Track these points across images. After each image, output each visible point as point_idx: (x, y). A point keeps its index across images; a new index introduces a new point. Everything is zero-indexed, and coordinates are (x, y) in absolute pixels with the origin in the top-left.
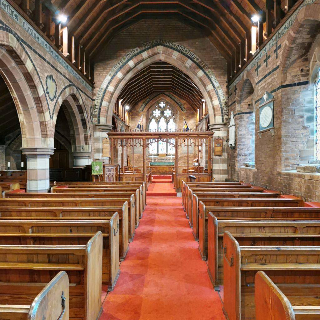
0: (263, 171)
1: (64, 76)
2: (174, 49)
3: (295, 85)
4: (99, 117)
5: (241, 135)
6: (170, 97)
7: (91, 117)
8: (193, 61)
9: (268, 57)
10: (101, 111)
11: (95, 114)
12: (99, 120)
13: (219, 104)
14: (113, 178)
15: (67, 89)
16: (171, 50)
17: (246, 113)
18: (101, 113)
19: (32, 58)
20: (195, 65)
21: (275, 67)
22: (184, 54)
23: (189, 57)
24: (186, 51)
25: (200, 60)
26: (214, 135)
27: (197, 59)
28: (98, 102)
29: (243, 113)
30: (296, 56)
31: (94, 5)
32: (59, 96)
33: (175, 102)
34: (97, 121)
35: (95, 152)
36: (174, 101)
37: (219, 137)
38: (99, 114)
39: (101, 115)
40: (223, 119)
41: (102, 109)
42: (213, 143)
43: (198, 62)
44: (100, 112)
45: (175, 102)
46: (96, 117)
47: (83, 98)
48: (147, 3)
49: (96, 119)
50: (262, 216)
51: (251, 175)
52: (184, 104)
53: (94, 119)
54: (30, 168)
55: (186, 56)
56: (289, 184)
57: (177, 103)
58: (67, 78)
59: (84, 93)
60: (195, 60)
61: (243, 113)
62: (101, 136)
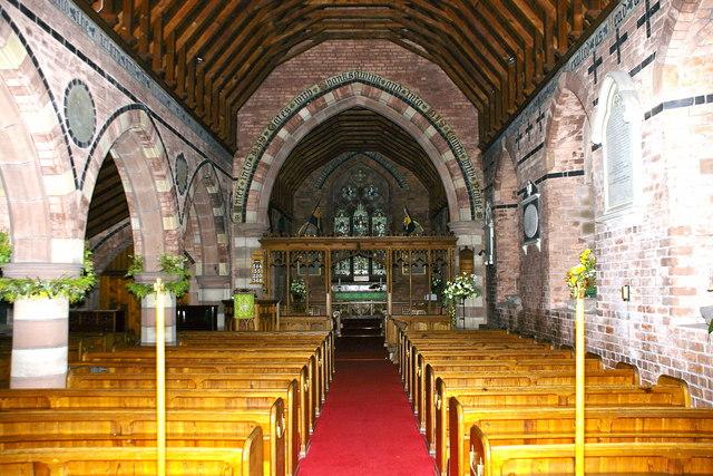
0: (529, 310)
1: (198, 151)
2: (382, 89)
3: (565, 174)
4: (245, 211)
5: (503, 244)
8: (417, 110)
9: (531, 127)
12: (244, 216)
15: (123, 116)
16: (376, 90)
17: (509, 206)
19: (23, 31)
20: (419, 116)
21: (539, 144)
22: (400, 97)
23: (409, 103)
24: (404, 92)
25: (428, 107)
27: (424, 107)
28: (242, 184)
29: (505, 207)
30: (566, 133)
31: (238, 10)
32: (101, 133)
38: (245, 205)
40: (473, 213)
42: (457, 258)
43: (425, 111)
44: (246, 201)
47: (221, 179)
49: (240, 214)
51: (515, 316)
54: (149, 306)
55: (405, 100)
56: (559, 328)
58: (200, 153)
59: (222, 171)
60: (421, 107)
61: (505, 207)
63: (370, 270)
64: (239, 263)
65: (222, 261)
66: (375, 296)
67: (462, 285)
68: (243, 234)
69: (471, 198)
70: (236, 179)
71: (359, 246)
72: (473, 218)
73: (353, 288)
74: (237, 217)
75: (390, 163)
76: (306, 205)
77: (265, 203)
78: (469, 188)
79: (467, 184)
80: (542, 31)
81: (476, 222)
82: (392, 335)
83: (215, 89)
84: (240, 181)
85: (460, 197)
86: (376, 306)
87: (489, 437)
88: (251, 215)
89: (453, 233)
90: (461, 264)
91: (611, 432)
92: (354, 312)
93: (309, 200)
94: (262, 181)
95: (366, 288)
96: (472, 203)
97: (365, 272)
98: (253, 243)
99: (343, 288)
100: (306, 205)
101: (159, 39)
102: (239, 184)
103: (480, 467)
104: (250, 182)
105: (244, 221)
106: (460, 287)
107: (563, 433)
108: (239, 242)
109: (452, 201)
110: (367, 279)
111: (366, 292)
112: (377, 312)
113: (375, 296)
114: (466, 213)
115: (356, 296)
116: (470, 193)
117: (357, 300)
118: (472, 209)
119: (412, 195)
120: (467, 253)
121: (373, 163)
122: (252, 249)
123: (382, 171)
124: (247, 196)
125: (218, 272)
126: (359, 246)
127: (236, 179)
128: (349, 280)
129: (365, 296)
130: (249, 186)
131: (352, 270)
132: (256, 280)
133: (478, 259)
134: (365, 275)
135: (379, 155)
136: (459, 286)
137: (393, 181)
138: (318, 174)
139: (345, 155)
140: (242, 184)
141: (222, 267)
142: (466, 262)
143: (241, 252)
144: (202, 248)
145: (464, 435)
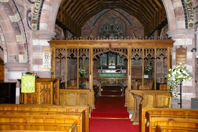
4: (39, 23)
6: (120, 13)
7: (29, 22)
10: (41, 16)
11: (35, 19)
12: (38, 26)
13: (182, 5)
14: (50, 96)
18: (41, 18)
26: (175, 44)
28: (37, 5)
33: (125, 17)
34: (36, 27)
35: (33, 63)
36: (123, 16)
37: (181, 46)
38: (39, 19)
39: (40, 21)
40: (186, 24)
41: (42, 13)
44: (39, 16)
45: (125, 17)
46: (35, 23)
48: (106, 118)
49: (36, 25)
50: (147, 106)
52: (133, 19)
53: (33, 25)
57: (126, 18)
62: (40, 45)
63: (116, 63)
64: (34, 55)
65: (21, 53)
66: (119, 75)
67: (181, 71)
68: (37, 37)
69: (185, 14)
70: (33, 3)
71: (110, 45)
72: (187, 27)
73: (108, 71)
74: (34, 27)
75: (126, 14)
76: (87, 33)
77: (53, 18)
78: (184, 7)
79: (183, 4)
80: (161, 8)
81: (190, 30)
82: (131, 101)
83: (79, 27)
84: (36, 4)
85: (176, 13)
86: (118, 80)
87: (151, 115)
88: (42, 25)
89: (170, 38)
90: (177, 58)
91: (188, 116)
92: (108, 83)
93: (88, 31)
94: (50, 4)
95: (114, 71)
96: (186, 17)
97: (114, 64)
98: (45, 43)
99: (103, 71)
100: (87, 33)
101: (65, 13)
102: (35, 6)
103: (148, 123)
104: (42, 4)
105: (38, 29)
106: (180, 73)
107: (171, 115)
108: (35, 42)
109: (170, 17)
110: (114, 67)
111: (114, 73)
112: (119, 83)
113: (119, 75)
114: (182, 24)
115: (109, 75)
116: (185, 10)
117: (110, 78)
118: (186, 21)
119: (136, 29)
120: (181, 50)
121: (118, 14)
122: (44, 47)
123: (122, 17)
124: (40, 13)
125: (18, 60)
126: (110, 45)
127: (33, 3)
128: (107, 68)
129: (114, 75)
130: (41, 7)
131: (108, 63)
132: (45, 67)
133: (190, 55)
134: (114, 66)
135: (121, 10)
136: (178, 72)
137: (127, 22)
138: (93, 19)
139: (105, 10)
140: (37, 5)
141: (21, 57)
142: (181, 56)
143: (36, 48)
144: (6, 45)
145: (143, 114)
